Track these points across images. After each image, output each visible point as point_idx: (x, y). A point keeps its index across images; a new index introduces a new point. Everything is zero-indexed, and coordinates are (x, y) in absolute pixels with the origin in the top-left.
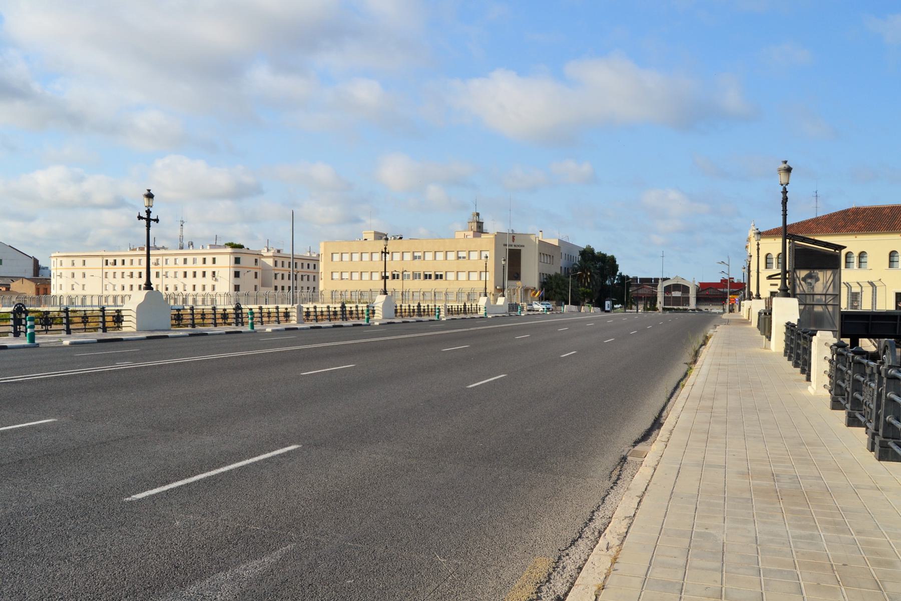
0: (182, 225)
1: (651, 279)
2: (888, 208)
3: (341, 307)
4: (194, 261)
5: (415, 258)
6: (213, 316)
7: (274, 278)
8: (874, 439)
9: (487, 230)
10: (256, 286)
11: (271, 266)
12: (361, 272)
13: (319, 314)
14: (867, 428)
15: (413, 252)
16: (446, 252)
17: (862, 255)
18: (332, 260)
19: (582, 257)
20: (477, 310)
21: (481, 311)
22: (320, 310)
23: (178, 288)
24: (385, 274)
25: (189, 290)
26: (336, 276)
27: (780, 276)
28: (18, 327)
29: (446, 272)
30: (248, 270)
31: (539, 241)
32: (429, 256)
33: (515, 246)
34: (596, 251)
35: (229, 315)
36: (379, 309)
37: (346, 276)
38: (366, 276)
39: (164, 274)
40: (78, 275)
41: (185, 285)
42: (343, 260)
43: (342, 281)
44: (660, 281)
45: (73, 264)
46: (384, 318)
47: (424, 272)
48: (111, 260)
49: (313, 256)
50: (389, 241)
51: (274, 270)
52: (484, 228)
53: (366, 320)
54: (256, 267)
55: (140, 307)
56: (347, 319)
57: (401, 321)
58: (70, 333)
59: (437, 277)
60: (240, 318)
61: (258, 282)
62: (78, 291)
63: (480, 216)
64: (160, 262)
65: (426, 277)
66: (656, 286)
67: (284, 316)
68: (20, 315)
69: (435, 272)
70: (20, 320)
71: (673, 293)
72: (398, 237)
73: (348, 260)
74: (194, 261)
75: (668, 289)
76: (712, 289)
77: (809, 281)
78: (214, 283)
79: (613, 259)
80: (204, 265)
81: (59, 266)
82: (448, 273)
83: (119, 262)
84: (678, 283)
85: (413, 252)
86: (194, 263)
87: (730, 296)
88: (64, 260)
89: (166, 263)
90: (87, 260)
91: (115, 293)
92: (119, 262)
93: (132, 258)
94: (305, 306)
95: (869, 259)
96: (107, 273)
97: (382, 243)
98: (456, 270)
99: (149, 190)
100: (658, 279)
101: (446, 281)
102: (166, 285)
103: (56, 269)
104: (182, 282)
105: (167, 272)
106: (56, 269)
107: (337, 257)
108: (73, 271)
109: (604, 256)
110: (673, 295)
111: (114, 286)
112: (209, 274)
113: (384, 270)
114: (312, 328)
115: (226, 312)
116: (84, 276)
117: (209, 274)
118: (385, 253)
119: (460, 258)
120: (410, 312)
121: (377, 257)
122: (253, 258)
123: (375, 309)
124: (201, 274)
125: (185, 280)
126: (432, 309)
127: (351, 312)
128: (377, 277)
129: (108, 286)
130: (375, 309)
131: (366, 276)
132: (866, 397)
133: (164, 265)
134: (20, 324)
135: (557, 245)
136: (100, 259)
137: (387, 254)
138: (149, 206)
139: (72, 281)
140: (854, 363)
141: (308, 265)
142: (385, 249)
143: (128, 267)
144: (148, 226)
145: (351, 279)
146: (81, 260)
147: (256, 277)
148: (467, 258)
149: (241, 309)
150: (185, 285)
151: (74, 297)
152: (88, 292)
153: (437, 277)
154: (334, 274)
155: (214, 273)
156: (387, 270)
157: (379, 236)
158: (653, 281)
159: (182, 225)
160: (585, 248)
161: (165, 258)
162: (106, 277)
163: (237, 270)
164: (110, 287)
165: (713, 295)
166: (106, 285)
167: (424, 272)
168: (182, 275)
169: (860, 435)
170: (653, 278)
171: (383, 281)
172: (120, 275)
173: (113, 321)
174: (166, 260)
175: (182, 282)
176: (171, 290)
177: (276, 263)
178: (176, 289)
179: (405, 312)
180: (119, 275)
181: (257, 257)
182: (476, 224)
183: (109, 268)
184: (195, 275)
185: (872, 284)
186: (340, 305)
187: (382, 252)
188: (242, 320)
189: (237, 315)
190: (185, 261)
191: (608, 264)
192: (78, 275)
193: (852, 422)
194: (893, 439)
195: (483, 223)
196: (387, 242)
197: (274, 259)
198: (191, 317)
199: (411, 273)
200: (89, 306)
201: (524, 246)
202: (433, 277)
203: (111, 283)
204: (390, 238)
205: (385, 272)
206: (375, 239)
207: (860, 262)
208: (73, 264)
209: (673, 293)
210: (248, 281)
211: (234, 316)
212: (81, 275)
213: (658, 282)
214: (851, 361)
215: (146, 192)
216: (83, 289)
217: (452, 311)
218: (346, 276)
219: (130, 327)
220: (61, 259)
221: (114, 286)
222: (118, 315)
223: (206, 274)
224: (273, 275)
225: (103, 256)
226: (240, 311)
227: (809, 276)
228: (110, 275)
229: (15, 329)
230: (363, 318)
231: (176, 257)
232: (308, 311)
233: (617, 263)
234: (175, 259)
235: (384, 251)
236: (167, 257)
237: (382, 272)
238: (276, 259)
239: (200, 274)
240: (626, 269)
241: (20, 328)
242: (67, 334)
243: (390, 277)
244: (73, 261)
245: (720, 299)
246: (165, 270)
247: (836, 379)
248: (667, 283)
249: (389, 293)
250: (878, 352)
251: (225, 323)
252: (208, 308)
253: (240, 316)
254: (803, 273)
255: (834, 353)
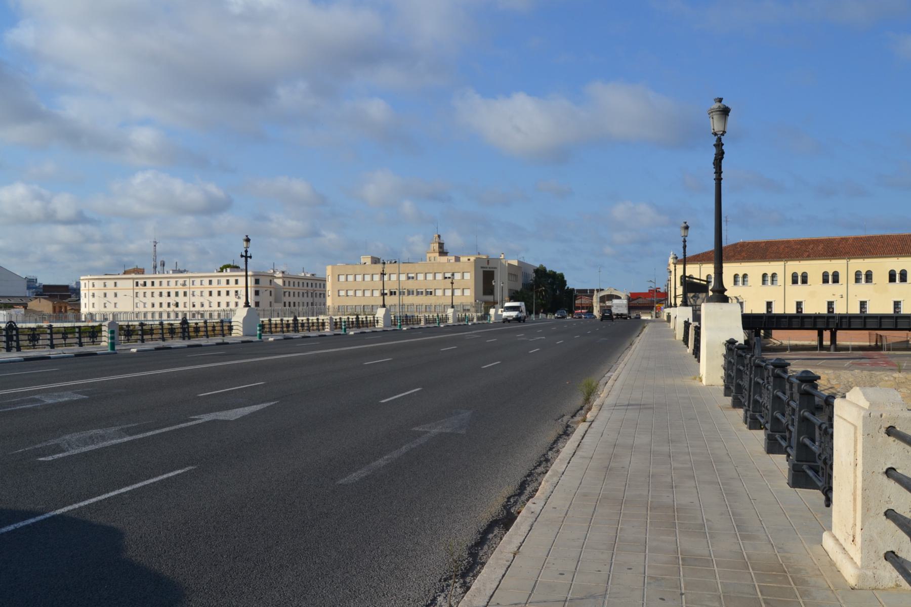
0: (155, 246)
1: (587, 290)
2: (764, 242)
3: (293, 320)
4: (219, 282)
5: (409, 278)
6: (160, 331)
7: (283, 295)
8: (747, 414)
9: (447, 250)
10: (271, 302)
11: (280, 285)
12: (364, 290)
13: (369, 322)
14: (789, 455)
15: (408, 274)
16: (435, 273)
17: (745, 276)
18: (339, 280)
19: (536, 274)
20: (374, 323)
21: (379, 324)
22: (274, 322)
23: (155, 305)
24: (384, 292)
25: (215, 307)
26: (342, 293)
27: (682, 296)
28: (10, 343)
29: (435, 289)
30: (266, 289)
31: (508, 264)
32: (421, 277)
33: (490, 268)
34: (548, 269)
35: (176, 329)
36: (381, 319)
37: (351, 293)
38: (368, 294)
39: (191, 293)
40: (110, 295)
41: (210, 303)
42: (348, 280)
43: (347, 297)
44: (595, 292)
45: (105, 286)
46: (245, 335)
47: (417, 290)
48: (141, 282)
49: (307, 275)
50: (386, 265)
51: (283, 288)
52: (445, 248)
53: (437, 324)
54: (270, 286)
55: (245, 319)
56: (298, 331)
57: (317, 335)
58: (144, 342)
59: (427, 293)
60: (15, 341)
61: (272, 299)
62: (110, 309)
63: (441, 238)
64: (187, 283)
65: (418, 293)
66: (591, 296)
67: (228, 329)
68: (12, 332)
69: (426, 289)
70: (12, 336)
71: (607, 302)
72: (394, 261)
73: (395, 280)
74: (219, 282)
75: (603, 299)
76: (641, 299)
77: (694, 298)
78: (237, 300)
79: (562, 276)
80: (228, 286)
81: (91, 287)
82: (437, 290)
83: (149, 283)
84: (612, 293)
85: (408, 274)
86: (218, 284)
87: (657, 305)
88: (96, 282)
89: (193, 284)
90: (119, 282)
91: (145, 310)
92: (149, 283)
93: (161, 280)
94: (285, 319)
95: (749, 279)
96: (137, 293)
97: (379, 267)
98: (443, 288)
99: (247, 236)
100: (594, 290)
101: (436, 297)
102: (193, 303)
103: (89, 290)
104: (208, 300)
105: (193, 292)
106: (89, 290)
107: (342, 278)
108: (115, 291)
109: (555, 273)
110: (607, 305)
111: (145, 304)
112: (232, 293)
113: (382, 288)
114: (157, 349)
115: (198, 326)
116: (116, 295)
117: (232, 293)
118: (383, 274)
119: (446, 278)
120: (318, 326)
121: (377, 278)
122: (269, 279)
123: (232, 324)
124: (225, 293)
125: (210, 298)
126: (403, 320)
127: (303, 325)
128: (377, 293)
129: (138, 304)
130: (232, 324)
131: (368, 294)
132: (764, 399)
133: (191, 286)
134: (12, 340)
135: (517, 265)
136: (131, 281)
137: (249, 259)
138: (247, 247)
139: (105, 300)
140: (755, 367)
141: (307, 283)
142: (246, 252)
143: (232, 289)
144: (246, 261)
145: (355, 296)
146: (112, 282)
147: (271, 295)
148: (415, 278)
149: (188, 323)
150: (210, 303)
151: (94, 314)
152: (120, 308)
153: (427, 293)
154: (340, 292)
155: (236, 292)
156: (385, 288)
157: (375, 261)
158: (588, 291)
159: (155, 246)
160: (538, 266)
161: (191, 280)
162: (137, 296)
163: (257, 289)
164: (141, 305)
165: (642, 304)
166: (137, 303)
167: (417, 290)
168: (208, 294)
169: (781, 463)
170: (588, 289)
171: (382, 297)
172: (142, 294)
173: (29, 340)
174: (193, 281)
175: (208, 300)
176: (198, 308)
177: (284, 282)
178: (202, 305)
179: (370, 323)
180: (149, 294)
181: (271, 278)
182: (437, 244)
183: (140, 289)
184: (219, 293)
185: (736, 298)
186: (355, 317)
187: (381, 274)
188: (189, 334)
189: (184, 329)
190: (210, 282)
191: (557, 280)
192: (110, 295)
193: (773, 447)
194: (806, 461)
195: (443, 244)
196: (384, 266)
197: (283, 280)
198: (160, 331)
199: (406, 291)
200: (150, 321)
201: (496, 268)
202: (424, 293)
203: (142, 302)
204: (386, 262)
205: (384, 290)
206: (372, 263)
207: (744, 281)
208: (105, 286)
209: (607, 302)
210: (265, 298)
211: (180, 330)
212: (113, 295)
213: (594, 293)
214: (752, 365)
215: (245, 238)
216: (115, 307)
217: (367, 323)
218: (351, 293)
219: (238, 332)
220: (93, 281)
221: (145, 304)
222: (34, 333)
223: (221, 293)
224: (283, 293)
225: (133, 279)
226: (186, 326)
227: (694, 296)
228: (141, 294)
229: (8, 345)
230: (436, 323)
231: (202, 279)
232: (197, 327)
233: (565, 279)
234: (201, 281)
235: (244, 254)
236: (193, 279)
237: (381, 290)
238: (285, 279)
239: (223, 293)
240: (572, 283)
241: (12, 344)
242: (51, 348)
243: (388, 294)
244: (105, 283)
245: (649, 308)
246: (192, 290)
247: (728, 370)
248: (602, 294)
249: (388, 307)
250: (455, 257)
251: (34, 345)
252: (201, 323)
253: (187, 330)
254: (691, 295)
255: (770, 374)
